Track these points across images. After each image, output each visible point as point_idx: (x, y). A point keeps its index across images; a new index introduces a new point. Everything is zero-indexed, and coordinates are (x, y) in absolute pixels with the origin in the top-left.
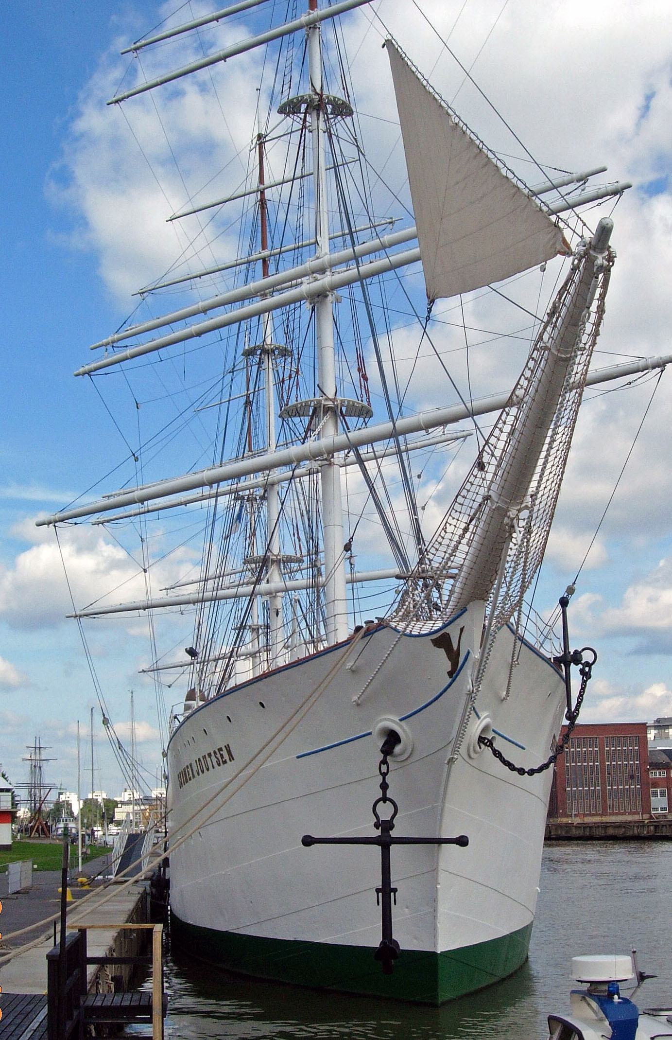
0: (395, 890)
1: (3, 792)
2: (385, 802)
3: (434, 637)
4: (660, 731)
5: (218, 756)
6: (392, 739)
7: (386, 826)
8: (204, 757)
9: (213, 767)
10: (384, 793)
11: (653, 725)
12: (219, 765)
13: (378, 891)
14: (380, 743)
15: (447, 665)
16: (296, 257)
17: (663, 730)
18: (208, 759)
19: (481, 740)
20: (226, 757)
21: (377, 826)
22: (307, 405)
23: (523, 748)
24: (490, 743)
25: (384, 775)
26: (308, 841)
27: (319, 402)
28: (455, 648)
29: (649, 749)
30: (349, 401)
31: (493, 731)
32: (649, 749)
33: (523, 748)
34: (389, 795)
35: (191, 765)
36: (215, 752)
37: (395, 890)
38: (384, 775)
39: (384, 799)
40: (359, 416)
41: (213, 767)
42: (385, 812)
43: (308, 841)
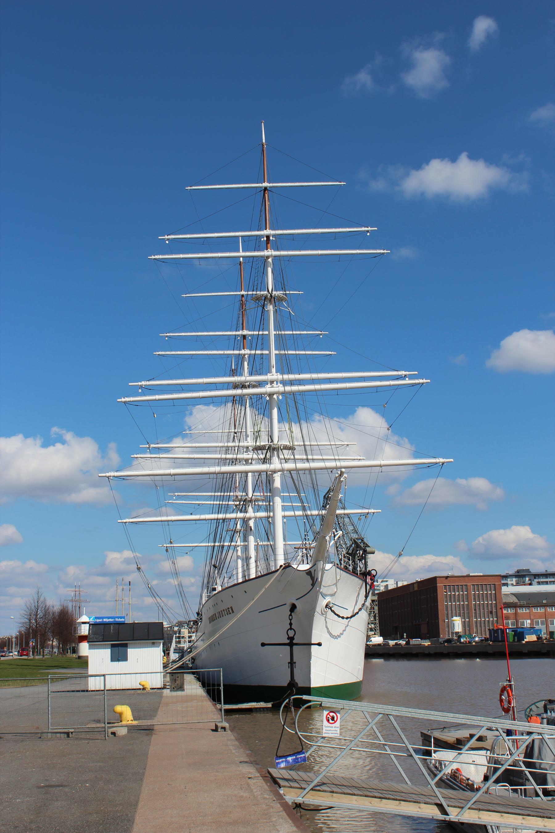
0: (295, 663)
1: (86, 624)
2: (291, 630)
3: (307, 571)
4: (519, 579)
5: (228, 611)
6: (293, 607)
7: (291, 639)
8: (221, 611)
9: (225, 615)
10: (291, 627)
11: (514, 574)
12: (228, 614)
13: (289, 663)
14: (289, 608)
15: (311, 582)
16: (258, 399)
17: (522, 579)
18: (223, 612)
19: (326, 606)
20: (231, 611)
21: (288, 638)
22: (265, 446)
23: (347, 609)
24: (331, 608)
25: (291, 620)
26: (263, 645)
27: (270, 446)
28: (313, 576)
29: (503, 593)
30: (284, 445)
31: (332, 603)
32: (503, 593)
33: (347, 609)
34: (292, 627)
35: (215, 614)
36: (226, 609)
37: (295, 663)
38: (291, 620)
39: (291, 629)
40: (289, 450)
41: (225, 615)
42: (291, 633)
43: (263, 645)
